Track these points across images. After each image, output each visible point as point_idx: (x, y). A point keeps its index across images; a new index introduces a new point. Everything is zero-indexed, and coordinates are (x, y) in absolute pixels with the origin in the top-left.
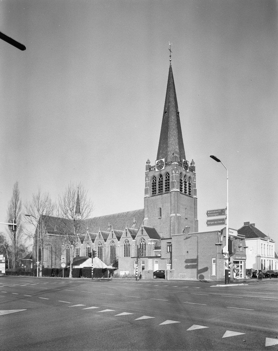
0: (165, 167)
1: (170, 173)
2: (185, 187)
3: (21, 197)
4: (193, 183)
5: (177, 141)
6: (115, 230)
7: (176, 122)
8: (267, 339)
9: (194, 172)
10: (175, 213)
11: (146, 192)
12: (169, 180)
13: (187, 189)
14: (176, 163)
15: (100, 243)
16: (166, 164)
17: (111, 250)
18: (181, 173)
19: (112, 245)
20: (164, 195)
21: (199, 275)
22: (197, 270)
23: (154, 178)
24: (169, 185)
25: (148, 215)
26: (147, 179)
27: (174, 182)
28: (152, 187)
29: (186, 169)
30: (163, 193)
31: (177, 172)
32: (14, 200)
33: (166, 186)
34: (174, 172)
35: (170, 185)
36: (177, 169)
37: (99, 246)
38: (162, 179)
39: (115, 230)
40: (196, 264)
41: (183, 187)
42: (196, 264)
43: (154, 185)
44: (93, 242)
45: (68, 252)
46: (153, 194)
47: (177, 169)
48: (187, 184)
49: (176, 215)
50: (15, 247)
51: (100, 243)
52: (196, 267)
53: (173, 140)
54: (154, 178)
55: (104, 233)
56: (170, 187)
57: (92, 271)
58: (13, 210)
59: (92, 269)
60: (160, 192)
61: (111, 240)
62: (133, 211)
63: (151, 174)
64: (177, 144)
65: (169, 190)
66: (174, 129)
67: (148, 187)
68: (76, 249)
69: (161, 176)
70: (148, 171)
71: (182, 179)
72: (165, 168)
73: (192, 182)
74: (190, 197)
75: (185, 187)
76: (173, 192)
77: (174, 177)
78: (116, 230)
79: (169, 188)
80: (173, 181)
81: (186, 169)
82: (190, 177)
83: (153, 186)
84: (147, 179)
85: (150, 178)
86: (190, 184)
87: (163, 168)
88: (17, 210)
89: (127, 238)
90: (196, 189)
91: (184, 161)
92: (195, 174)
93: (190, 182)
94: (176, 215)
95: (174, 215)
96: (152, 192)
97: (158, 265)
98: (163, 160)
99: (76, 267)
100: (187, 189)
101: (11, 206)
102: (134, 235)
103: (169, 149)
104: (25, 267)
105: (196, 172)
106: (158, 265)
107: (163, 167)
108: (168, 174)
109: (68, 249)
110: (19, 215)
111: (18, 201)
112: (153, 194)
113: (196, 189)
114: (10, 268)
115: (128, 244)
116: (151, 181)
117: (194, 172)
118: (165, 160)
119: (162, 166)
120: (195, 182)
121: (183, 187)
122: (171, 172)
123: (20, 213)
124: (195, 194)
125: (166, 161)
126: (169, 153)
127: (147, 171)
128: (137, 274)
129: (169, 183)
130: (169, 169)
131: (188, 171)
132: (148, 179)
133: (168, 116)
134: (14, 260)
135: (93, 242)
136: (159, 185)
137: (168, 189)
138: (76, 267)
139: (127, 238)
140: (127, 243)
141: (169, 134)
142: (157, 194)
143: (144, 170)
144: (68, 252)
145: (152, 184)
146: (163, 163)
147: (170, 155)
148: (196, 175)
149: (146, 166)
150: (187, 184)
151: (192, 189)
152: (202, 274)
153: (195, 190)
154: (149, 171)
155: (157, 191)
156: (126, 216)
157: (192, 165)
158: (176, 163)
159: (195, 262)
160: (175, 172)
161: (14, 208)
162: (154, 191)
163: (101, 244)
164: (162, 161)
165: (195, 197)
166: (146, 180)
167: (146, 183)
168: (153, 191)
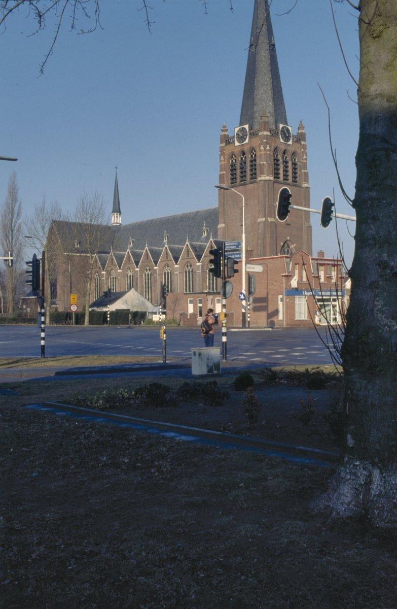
0: (250, 138)
1: (257, 149)
2: (286, 171)
3: (20, 195)
4: (301, 162)
5: (270, 93)
6: (171, 245)
7: (269, 62)
8: (297, 318)
9: (302, 142)
10: (265, 217)
11: (222, 178)
12: (255, 160)
13: (290, 173)
14: (266, 133)
15: (148, 268)
16: (251, 134)
17: (186, 283)
18: (276, 148)
19: (166, 271)
20: (248, 186)
21: (269, 321)
22: (268, 311)
23: (253, 151)
24: (255, 169)
25: (224, 220)
26: (222, 159)
27: (263, 164)
28: (230, 172)
29: (287, 138)
30: (247, 183)
31: (268, 148)
32: (10, 202)
33: (251, 170)
34: (262, 148)
35: (257, 169)
36: (267, 143)
37: (147, 273)
38: (245, 158)
39: (171, 245)
40: (266, 304)
41: (281, 171)
42: (266, 304)
43: (233, 168)
44: (176, 262)
45: (148, 287)
46: (232, 183)
47: (267, 143)
48: (290, 164)
49: (266, 220)
50: (12, 277)
51: (148, 268)
52: (265, 308)
53: (264, 92)
54: (253, 151)
55: (154, 250)
56: (257, 174)
57: (108, 316)
58: (8, 218)
59: (108, 313)
60: (242, 181)
61: (165, 263)
62: (205, 211)
63: (229, 150)
64: (270, 98)
65: (256, 178)
66: (265, 74)
67: (224, 172)
68: (111, 278)
69: (244, 154)
70: (224, 144)
71: (280, 157)
72: (249, 141)
73: (299, 161)
74: (296, 186)
75: (286, 171)
76: (261, 182)
77: (263, 156)
78: (173, 246)
79: (255, 174)
80: (262, 163)
81: (287, 138)
82: (294, 153)
83: (232, 170)
84: (222, 159)
85: (226, 157)
86: (294, 164)
87: (247, 141)
88: (15, 217)
89: (189, 260)
90: (307, 173)
91: (283, 128)
92: (304, 147)
93: (296, 161)
94: (266, 220)
95: (263, 219)
96: (250, 176)
97: (192, 305)
98: (247, 127)
99: (98, 310)
100: (290, 173)
101: (5, 211)
102: (177, 256)
103: (256, 108)
104: (29, 310)
105: (307, 142)
106: (192, 305)
107: (245, 139)
108: (252, 150)
109: (98, 278)
110: (17, 225)
111: (15, 203)
112: (232, 183)
113: (307, 173)
114: (5, 312)
115: (191, 270)
116: (228, 161)
117: (302, 142)
118: (249, 127)
119: (245, 137)
120: (306, 159)
121: (281, 171)
122: (258, 149)
123: (19, 221)
124: (307, 180)
125: (251, 128)
126: (257, 115)
127: (221, 145)
128: (160, 319)
129: (255, 165)
130: (256, 142)
131: (290, 142)
132: (224, 157)
133: (256, 51)
134: (10, 298)
135: (176, 262)
136: (240, 171)
137: (254, 176)
138: (98, 310)
139: (189, 260)
140: (189, 267)
141: (256, 82)
142: (237, 184)
143: (219, 145)
144: (148, 287)
145: (230, 167)
146: (246, 132)
147: (258, 119)
148: (308, 147)
149: (221, 136)
150: (290, 164)
151: (298, 172)
152: (273, 319)
153: (306, 174)
154: (226, 144)
155: (238, 179)
156: (193, 218)
157: (300, 131)
158: (266, 133)
159: (264, 302)
160: (265, 148)
161: (9, 215)
162: (233, 179)
163: (191, 266)
164: (245, 129)
165: (305, 185)
166: (220, 161)
167: (221, 165)
168: (232, 179)
